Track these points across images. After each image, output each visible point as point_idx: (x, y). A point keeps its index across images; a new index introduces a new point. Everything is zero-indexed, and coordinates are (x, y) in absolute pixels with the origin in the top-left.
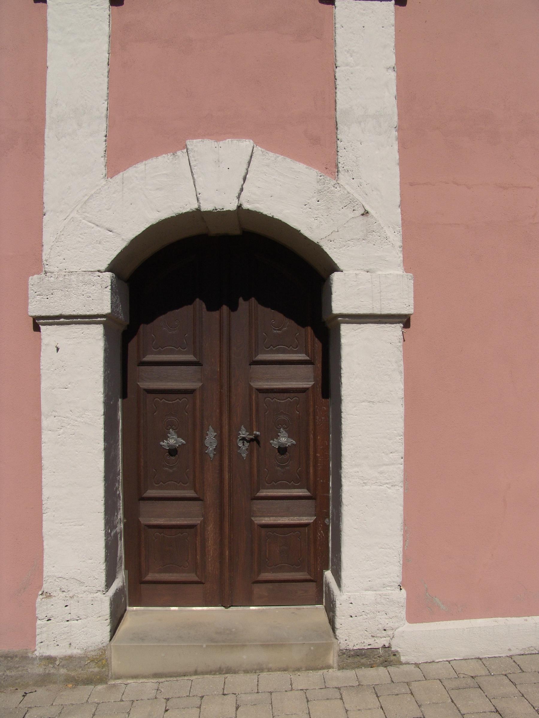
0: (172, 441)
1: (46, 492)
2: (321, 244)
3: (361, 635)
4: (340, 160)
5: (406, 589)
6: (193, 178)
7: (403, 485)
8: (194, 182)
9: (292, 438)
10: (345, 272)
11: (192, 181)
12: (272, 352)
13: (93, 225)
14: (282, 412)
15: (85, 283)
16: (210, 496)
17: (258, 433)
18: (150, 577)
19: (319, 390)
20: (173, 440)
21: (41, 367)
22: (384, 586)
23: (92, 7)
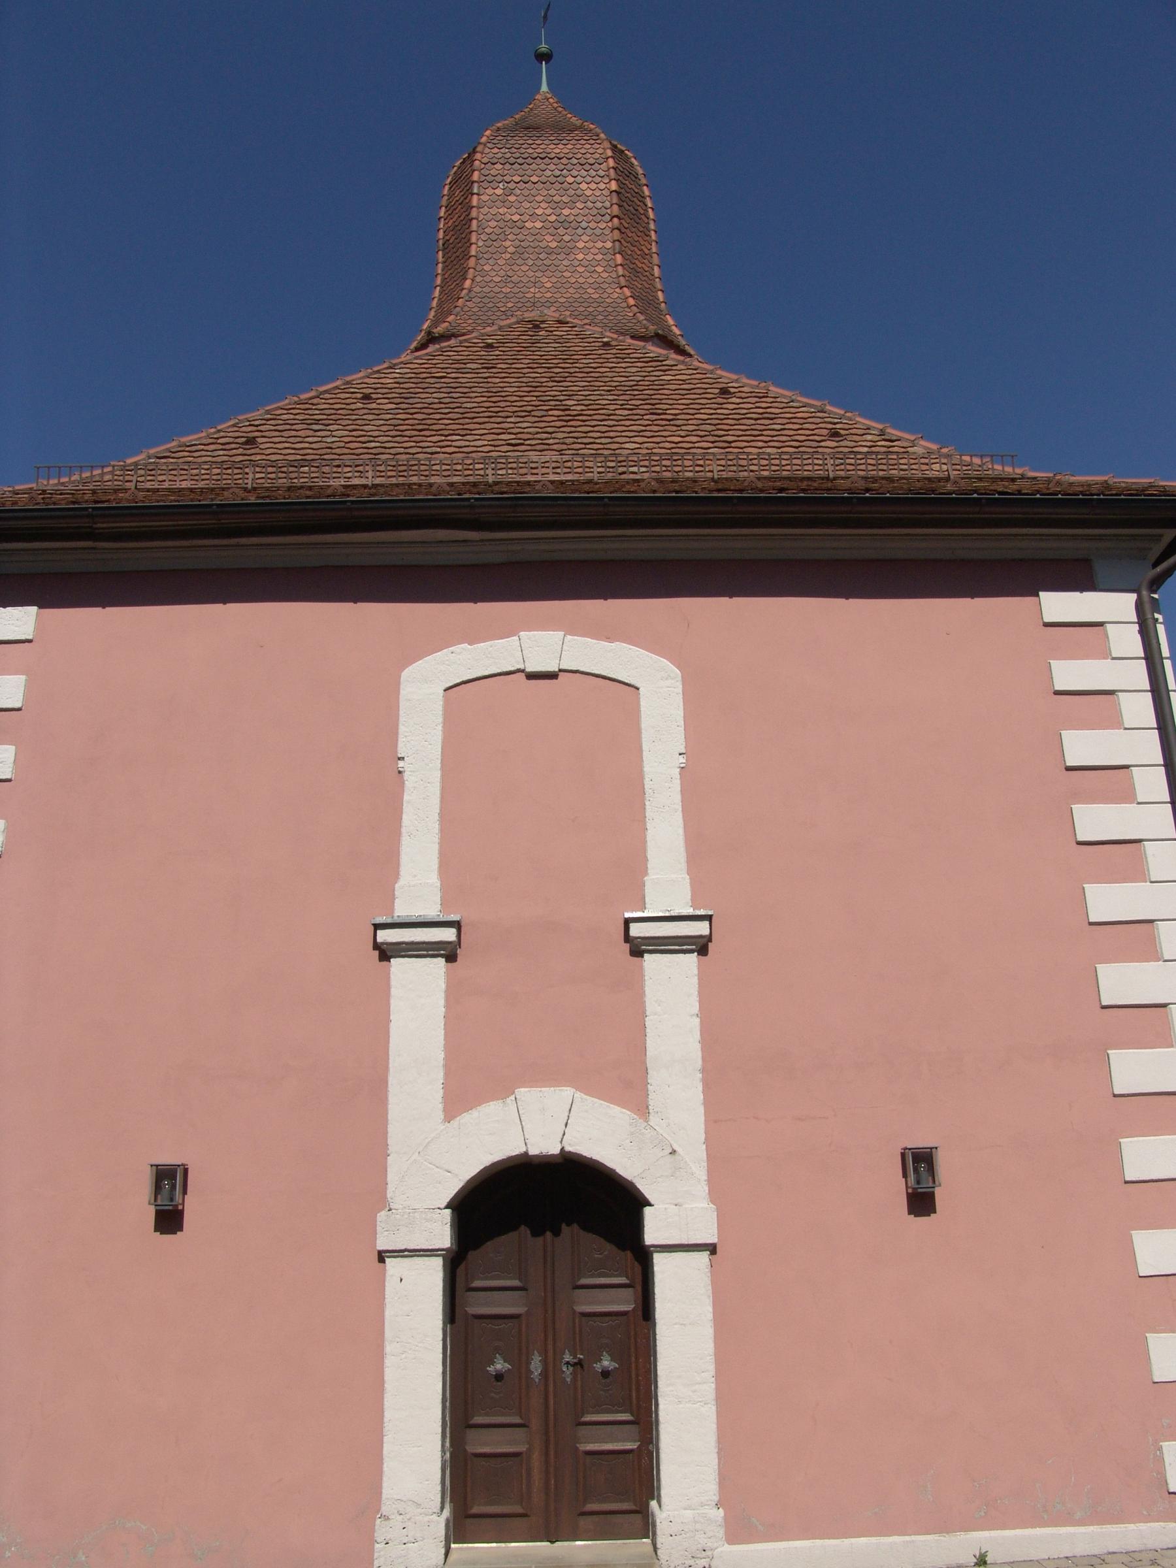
0: (499, 1367)
1: (388, 1415)
2: (634, 1181)
3: (682, 1556)
4: (651, 1102)
5: (723, 1509)
6: (522, 1124)
7: (715, 1403)
8: (522, 1128)
9: (615, 1362)
10: (655, 1206)
11: (520, 1126)
12: (592, 1276)
13: (434, 1167)
14: (604, 1336)
15: (427, 1220)
16: (536, 1423)
17: (581, 1357)
18: (475, 1510)
19: (640, 1313)
20: (500, 1365)
21: (386, 1297)
22: (702, 1505)
23: (431, 966)
